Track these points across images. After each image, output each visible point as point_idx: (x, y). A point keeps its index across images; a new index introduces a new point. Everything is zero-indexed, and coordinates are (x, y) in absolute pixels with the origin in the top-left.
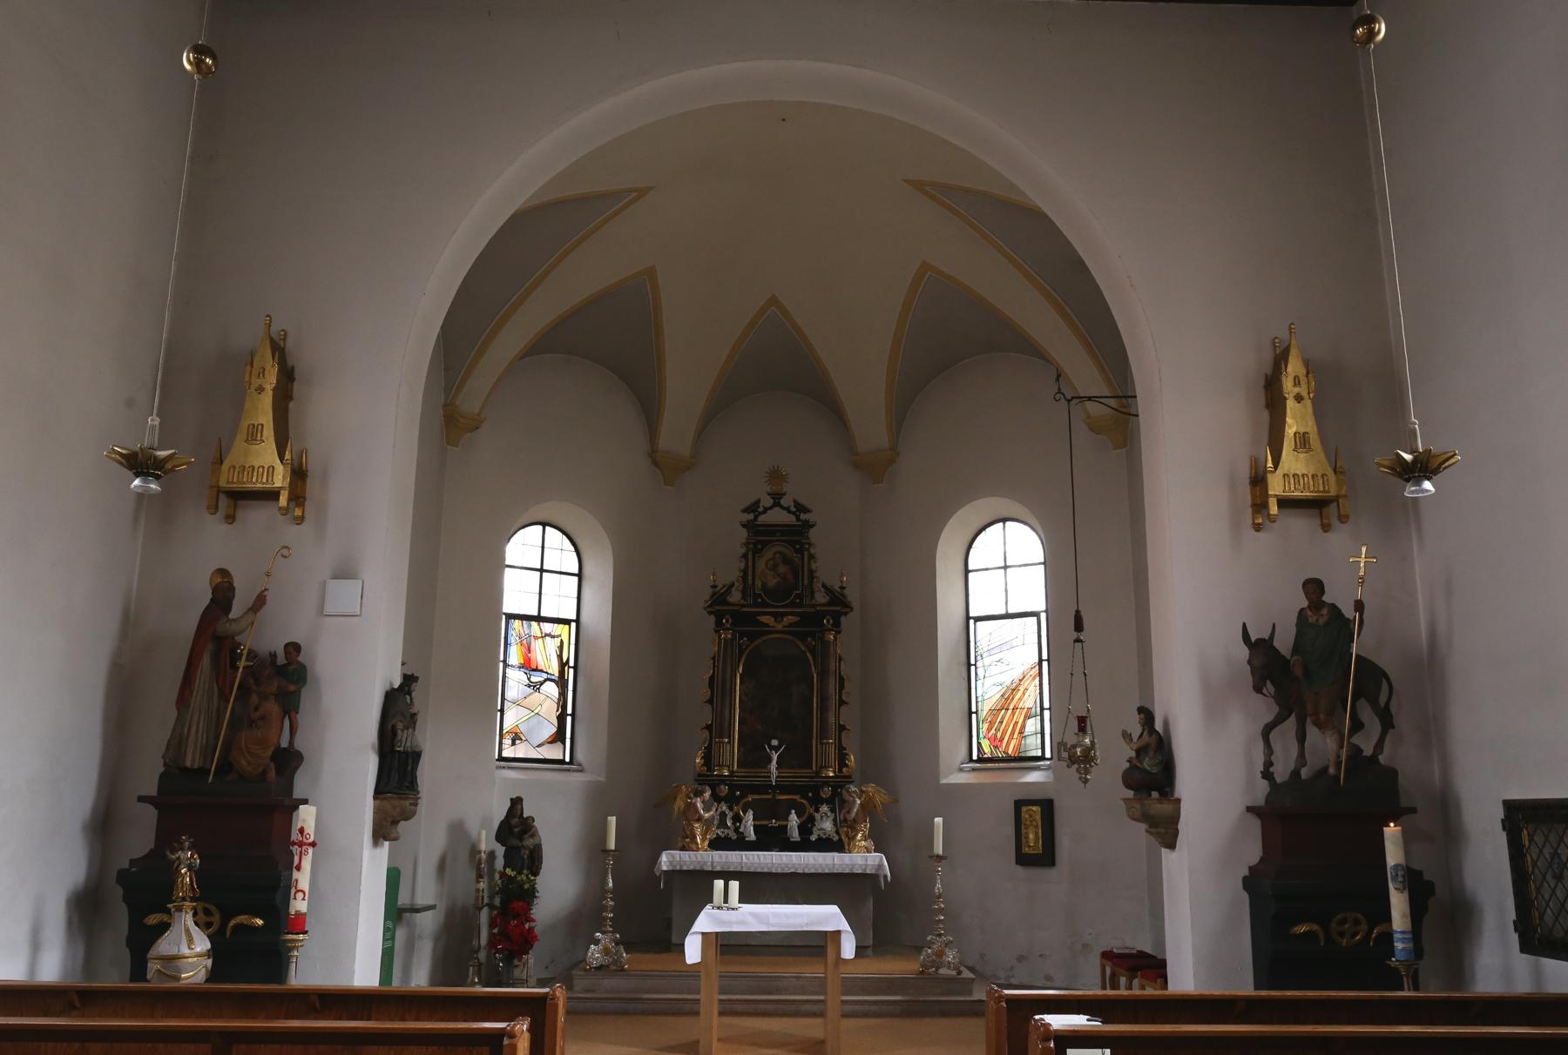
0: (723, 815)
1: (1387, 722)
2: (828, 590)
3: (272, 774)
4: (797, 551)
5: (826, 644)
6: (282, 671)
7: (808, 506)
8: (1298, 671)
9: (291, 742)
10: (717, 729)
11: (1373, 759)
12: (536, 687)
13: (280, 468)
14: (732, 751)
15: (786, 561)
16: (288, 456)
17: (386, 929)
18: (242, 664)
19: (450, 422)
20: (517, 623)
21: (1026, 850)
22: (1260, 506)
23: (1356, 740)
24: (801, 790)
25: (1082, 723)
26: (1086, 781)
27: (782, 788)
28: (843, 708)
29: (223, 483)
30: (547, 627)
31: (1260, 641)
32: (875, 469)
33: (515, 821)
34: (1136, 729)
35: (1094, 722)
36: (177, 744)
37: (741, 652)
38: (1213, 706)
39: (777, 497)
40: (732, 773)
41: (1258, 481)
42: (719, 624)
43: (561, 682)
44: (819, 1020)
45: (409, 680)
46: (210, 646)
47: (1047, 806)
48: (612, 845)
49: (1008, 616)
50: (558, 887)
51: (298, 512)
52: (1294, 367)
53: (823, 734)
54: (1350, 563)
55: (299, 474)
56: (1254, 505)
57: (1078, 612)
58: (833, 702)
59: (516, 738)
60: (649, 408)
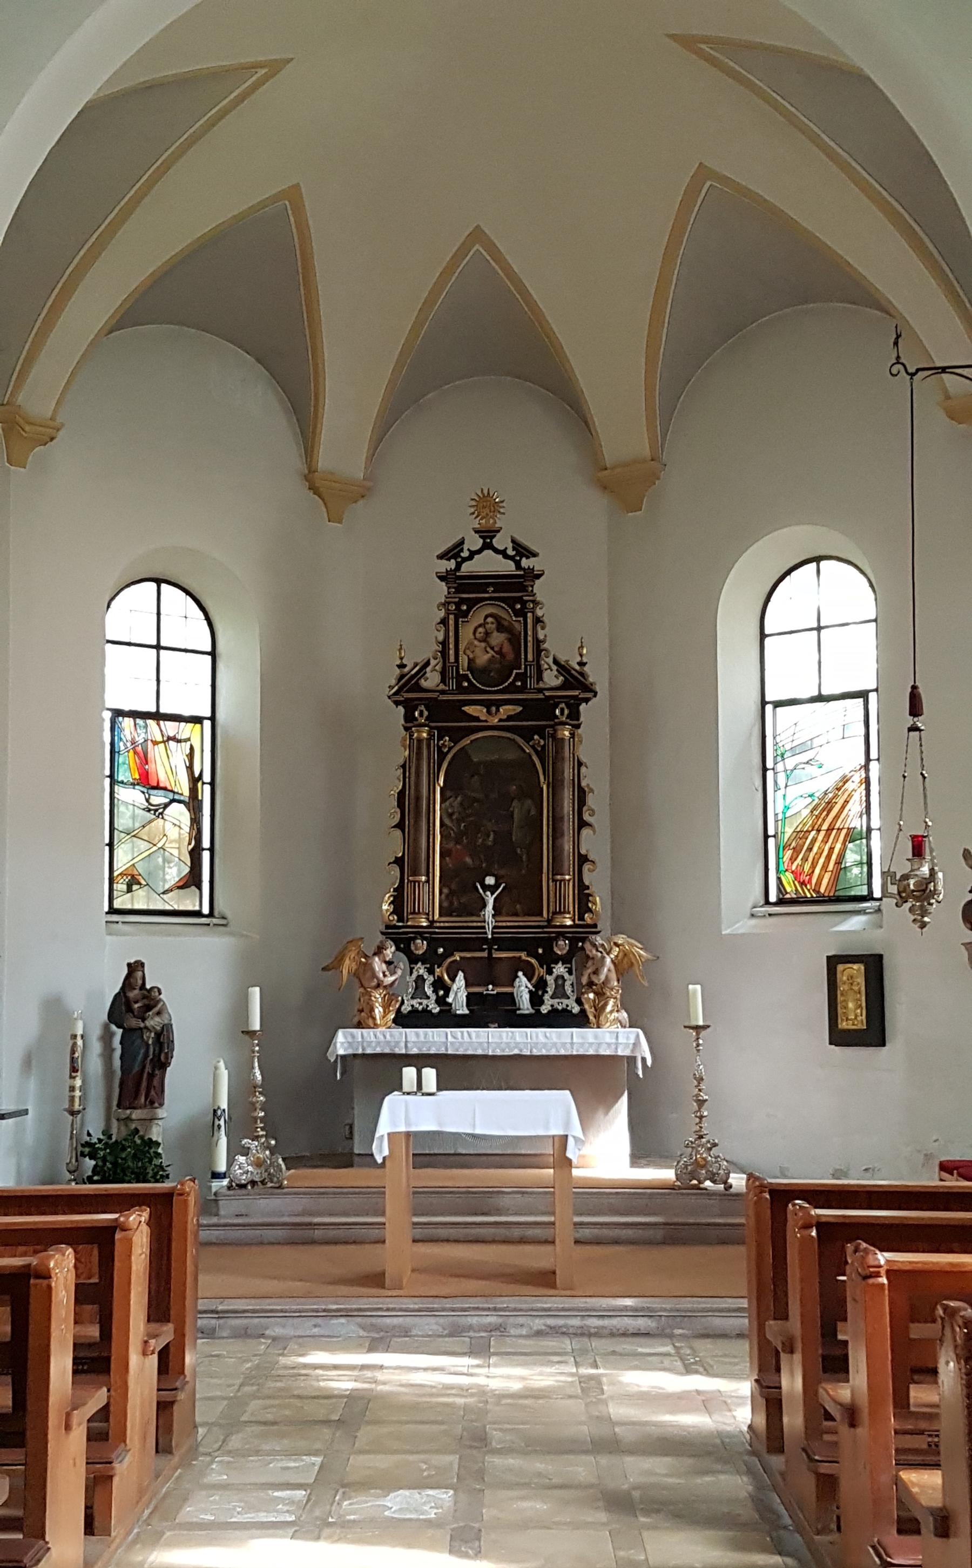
0: (420, 980)
2: (563, 668)
4: (517, 613)
5: (559, 742)
7: (534, 548)
12: (158, 811)
14: (431, 895)
15: (500, 628)
20: (127, 723)
21: (843, 1025)
24: (528, 945)
26: (923, 925)
27: (500, 942)
28: (585, 832)
30: (171, 728)
32: (626, 488)
33: (132, 994)
35: (931, 842)
37: (442, 756)
39: (487, 535)
40: (432, 922)
42: (409, 717)
43: (194, 804)
44: (549, 1248)
47: (874, 965)
48: (256, 1025)
49: (820, 698)
50: (200, 1078)
53: (557, 869)
57: (914, 687)
58: (568, 826)
59: (133, 882)
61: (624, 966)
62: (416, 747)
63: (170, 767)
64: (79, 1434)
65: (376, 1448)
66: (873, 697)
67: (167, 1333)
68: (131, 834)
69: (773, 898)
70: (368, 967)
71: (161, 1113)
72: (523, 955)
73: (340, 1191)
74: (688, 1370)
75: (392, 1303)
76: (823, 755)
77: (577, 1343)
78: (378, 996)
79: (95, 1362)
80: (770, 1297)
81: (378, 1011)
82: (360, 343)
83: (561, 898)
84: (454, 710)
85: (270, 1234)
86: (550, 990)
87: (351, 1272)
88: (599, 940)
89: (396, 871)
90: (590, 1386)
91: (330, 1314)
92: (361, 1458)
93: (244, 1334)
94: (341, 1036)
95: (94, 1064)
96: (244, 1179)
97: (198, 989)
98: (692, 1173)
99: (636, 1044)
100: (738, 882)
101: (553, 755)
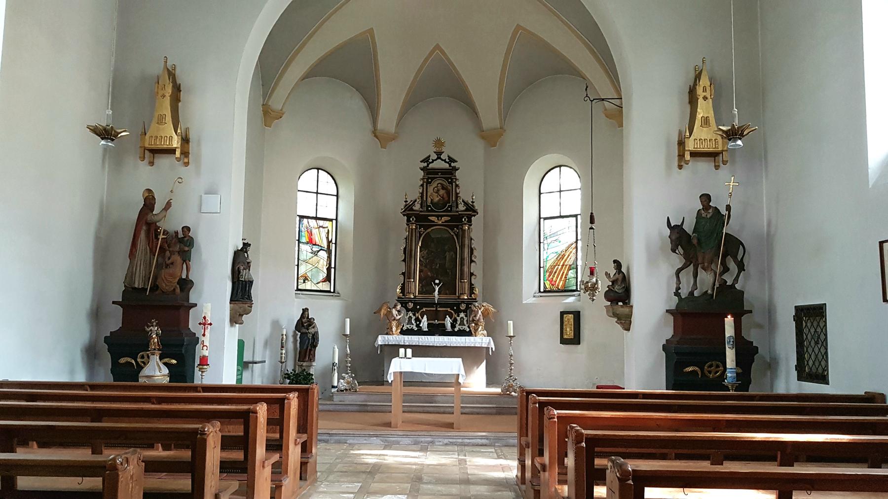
0: (410, 318)
1: (741, 267)
2: (466, 203)
3: (178, 290)
4: (449, 183)
6: (181, 241)
8: (695, 241)
9: (187, 276)
10: (407, 275)
11: (732, 286)
12: (315, 253)
13: (175, 137)
14: (415, 287)
15: (443, 188)
16: (179, 131)
17: (238, 370)
18: (161, 236)
19: (266, 114)
21: (565, 337)
22: (681, 156)
23: (725, 277)
24: (451, 306)
25: (592, 273)
26: (593, 300)
29: (147, 145)
30: (321, 223)
31: (676, 226)
32: (492, 139)
34: (613, 272)
35: (597, 270)
36: (130, 276)
38: (652, 260)
39: (439, 154)
40: (415, 297)
41: (681, 143)
42: (408, 220)
43: (329, 251)
45: (246, 245)
46: (144, 228)
47: (577, 315)
48: (348, 333)
49: (561, 217)
50: (329, 351)
51: (186, 160)
52: (704, 81)
53: (462, 278)
54: (724, 186)
55: (185, 140)
56: (679, 155)
58: (467, 262)
59: (306, 280)
60: (373, 109)
61: (485, 314)
62: (411, 231)
63: (320, 238)
64: (268, 470)
65: (382, 481)
66: (579, 217)
67: (304, 437)
68: (306, 261)
69: (542, 290)
70: (391, 312)
71: (314, 364)
72: (449, 310)
73: (377, 393)
74: (499, 457)
75: (393, 433)
76: (561, 238)
77: (459, 448)
78: (394, 323)
79: (276, 446)
80: (523, 430)
81: (394, 329)
82: (394, 83)
83: (463, 289)
84: (425, 218)
85: (350, 408)
86: (458, 322)
87: (378, 421)
88: (477, 304)
89: (402, 277)
90: (462, 462)
91: (370, 436)
92: (375, 484)
93: (338, 442)
94: (380, 338)
95: (290, 345)
96: (343, 388)
97: (329, 321)
98: (507, 390)
99: (489, 343)
100: (529, 284)
101: (461, 235)
